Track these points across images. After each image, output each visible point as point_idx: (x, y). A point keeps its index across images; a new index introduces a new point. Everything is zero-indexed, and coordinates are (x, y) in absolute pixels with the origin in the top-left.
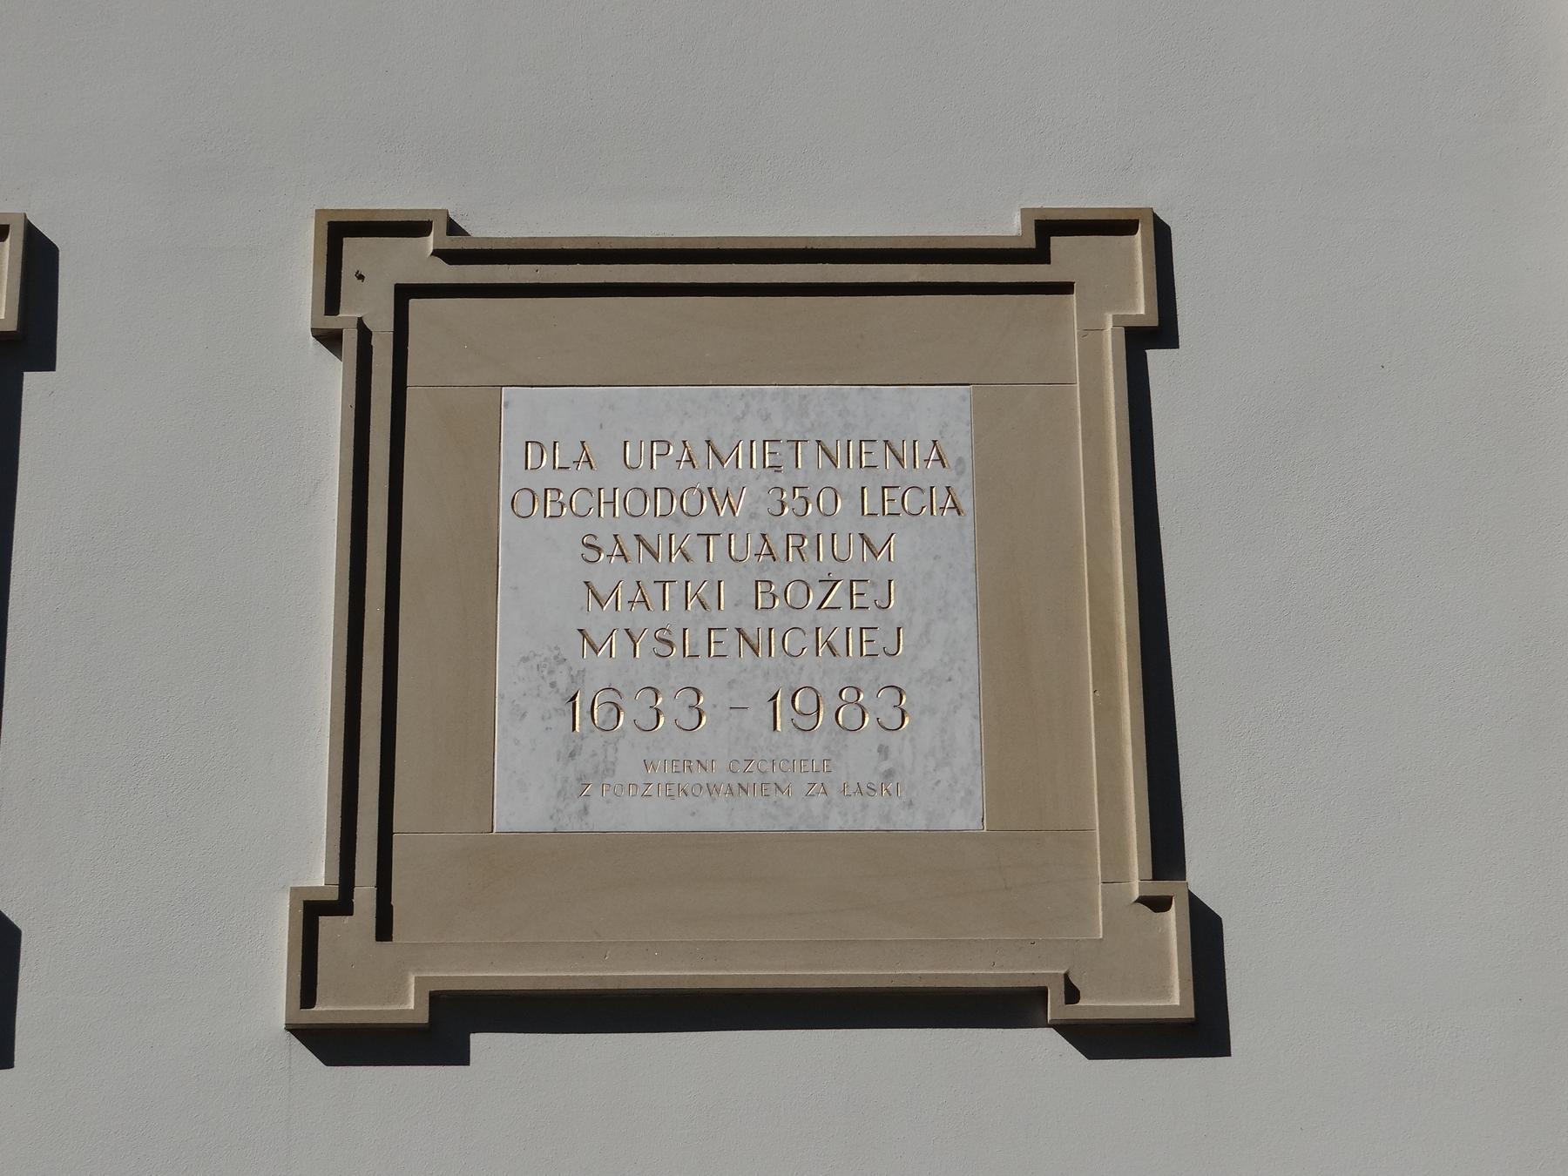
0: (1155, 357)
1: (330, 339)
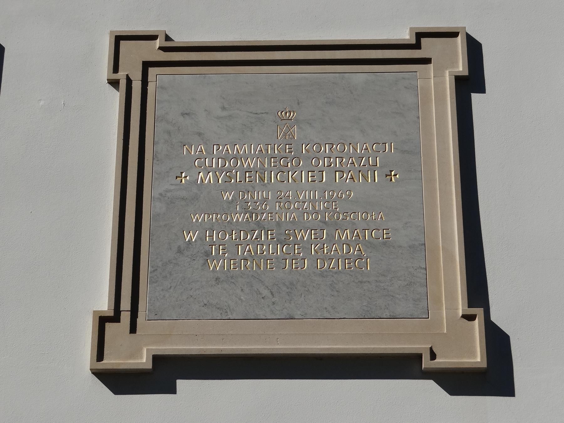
0: (475, 97)
1: (114, 83)
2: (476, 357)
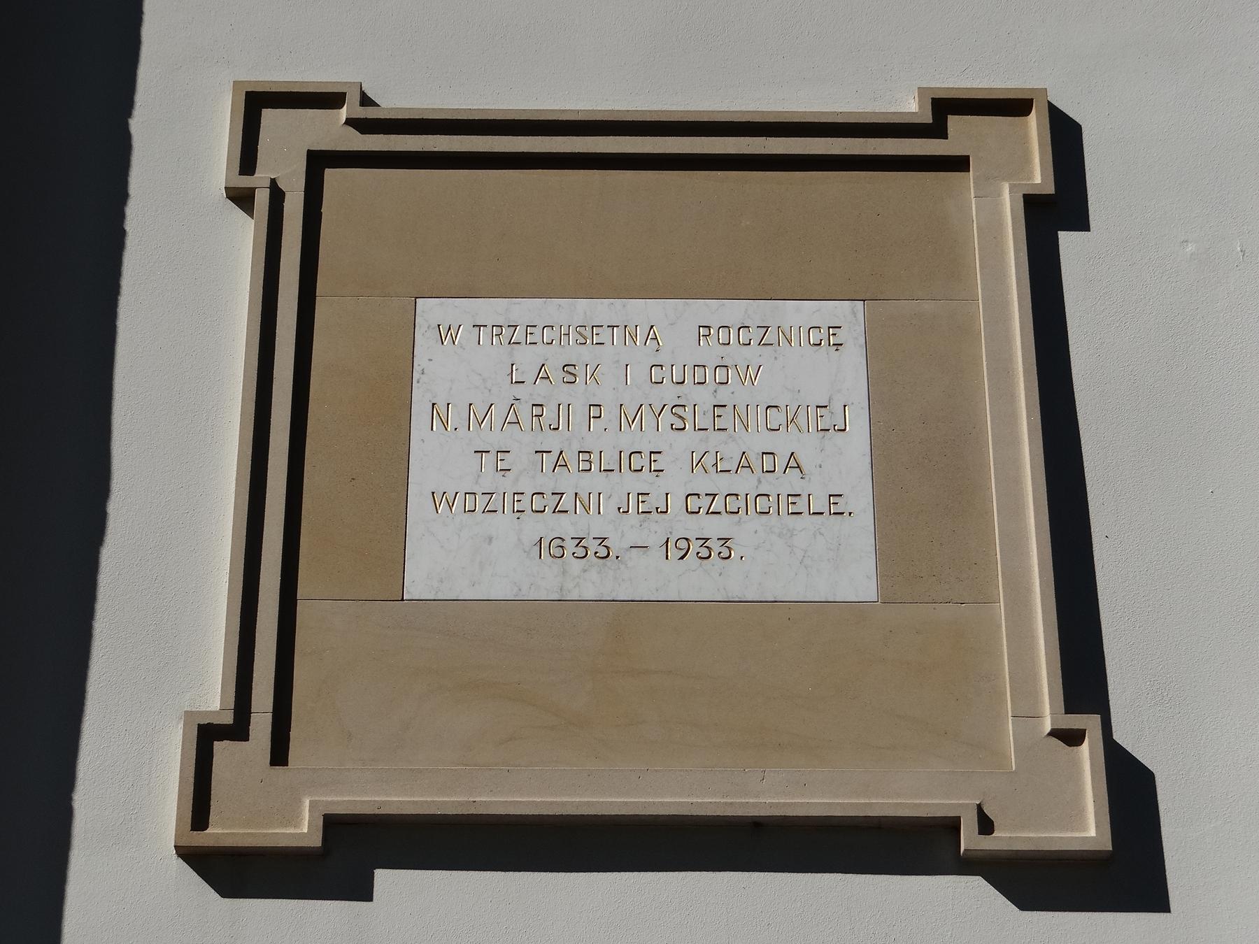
0: (1067, 239)
1: (242, 199)
2: (1089, 828)
